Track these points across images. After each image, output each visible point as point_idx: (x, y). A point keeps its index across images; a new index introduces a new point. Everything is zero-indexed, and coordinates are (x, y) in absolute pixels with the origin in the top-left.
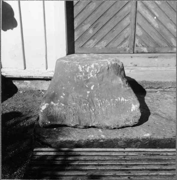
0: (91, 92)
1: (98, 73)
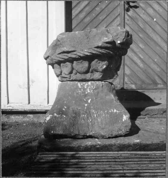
0: (89, 105)
1: (94, 89)
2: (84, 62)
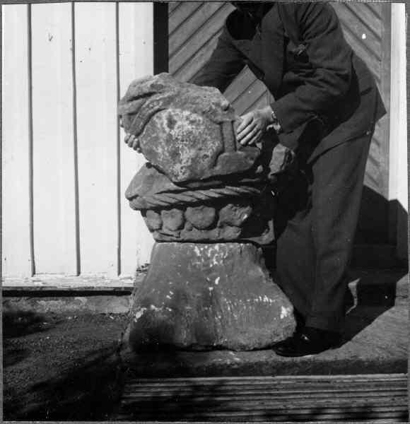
2: (206, 208)
